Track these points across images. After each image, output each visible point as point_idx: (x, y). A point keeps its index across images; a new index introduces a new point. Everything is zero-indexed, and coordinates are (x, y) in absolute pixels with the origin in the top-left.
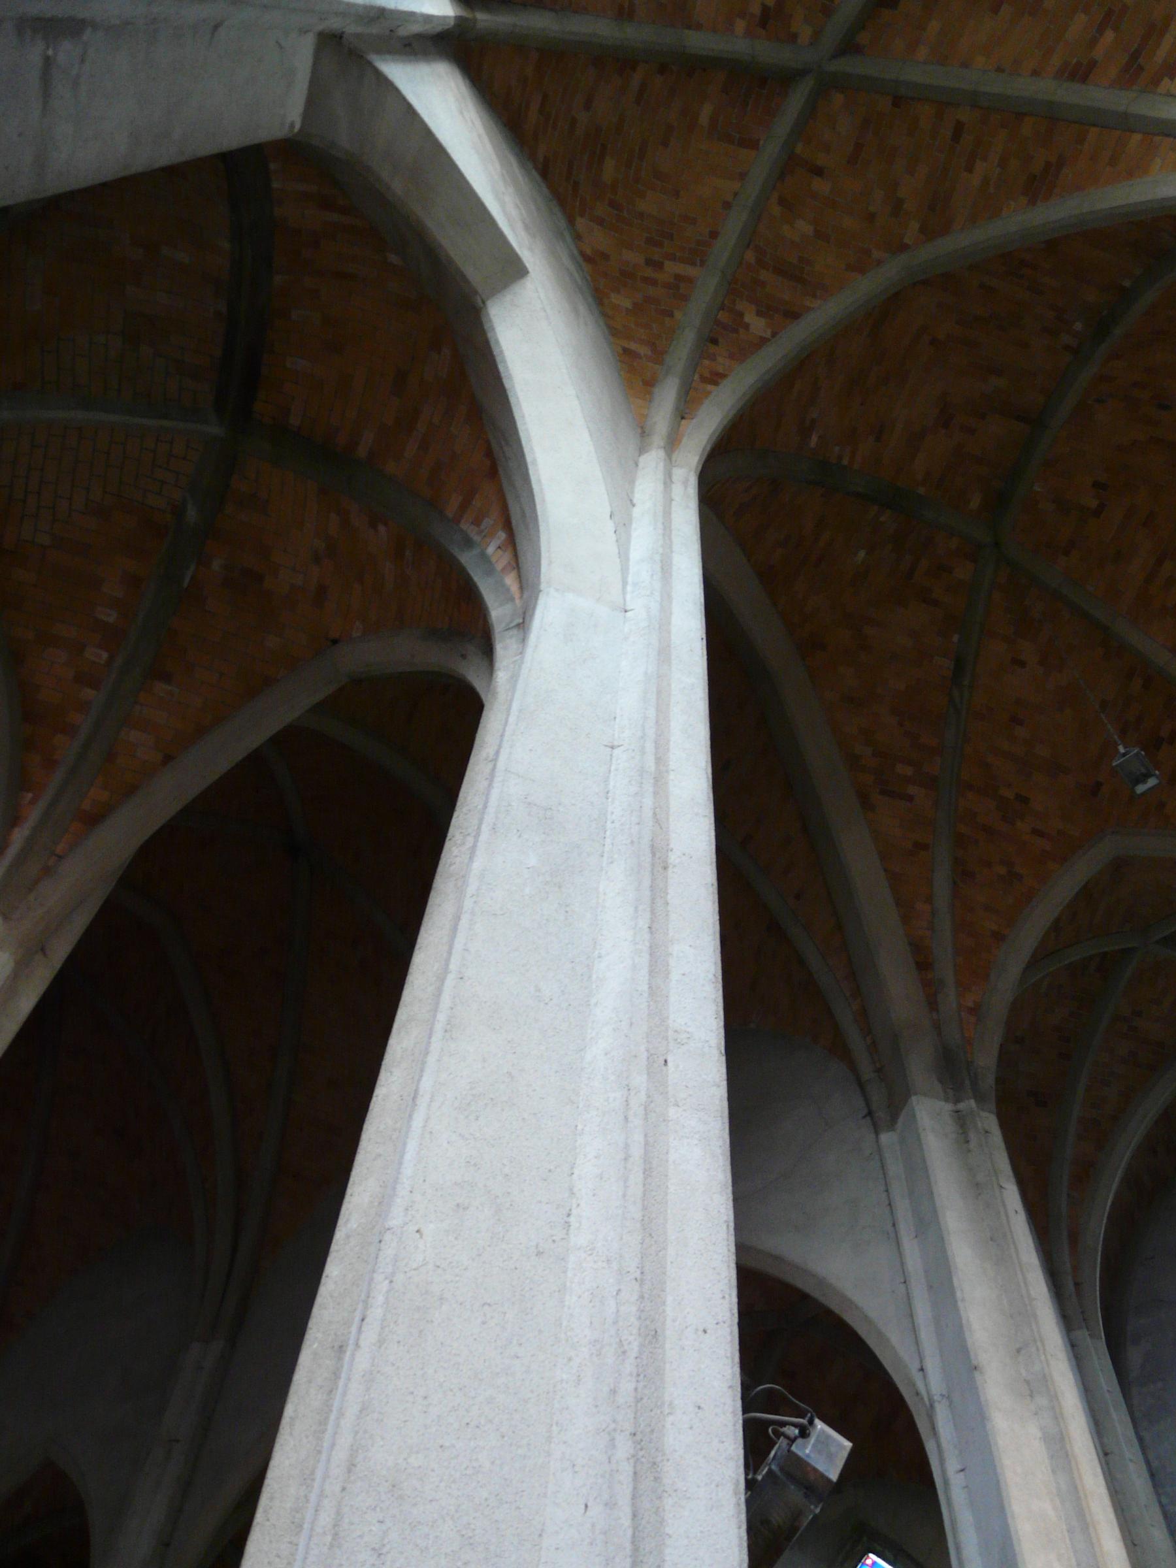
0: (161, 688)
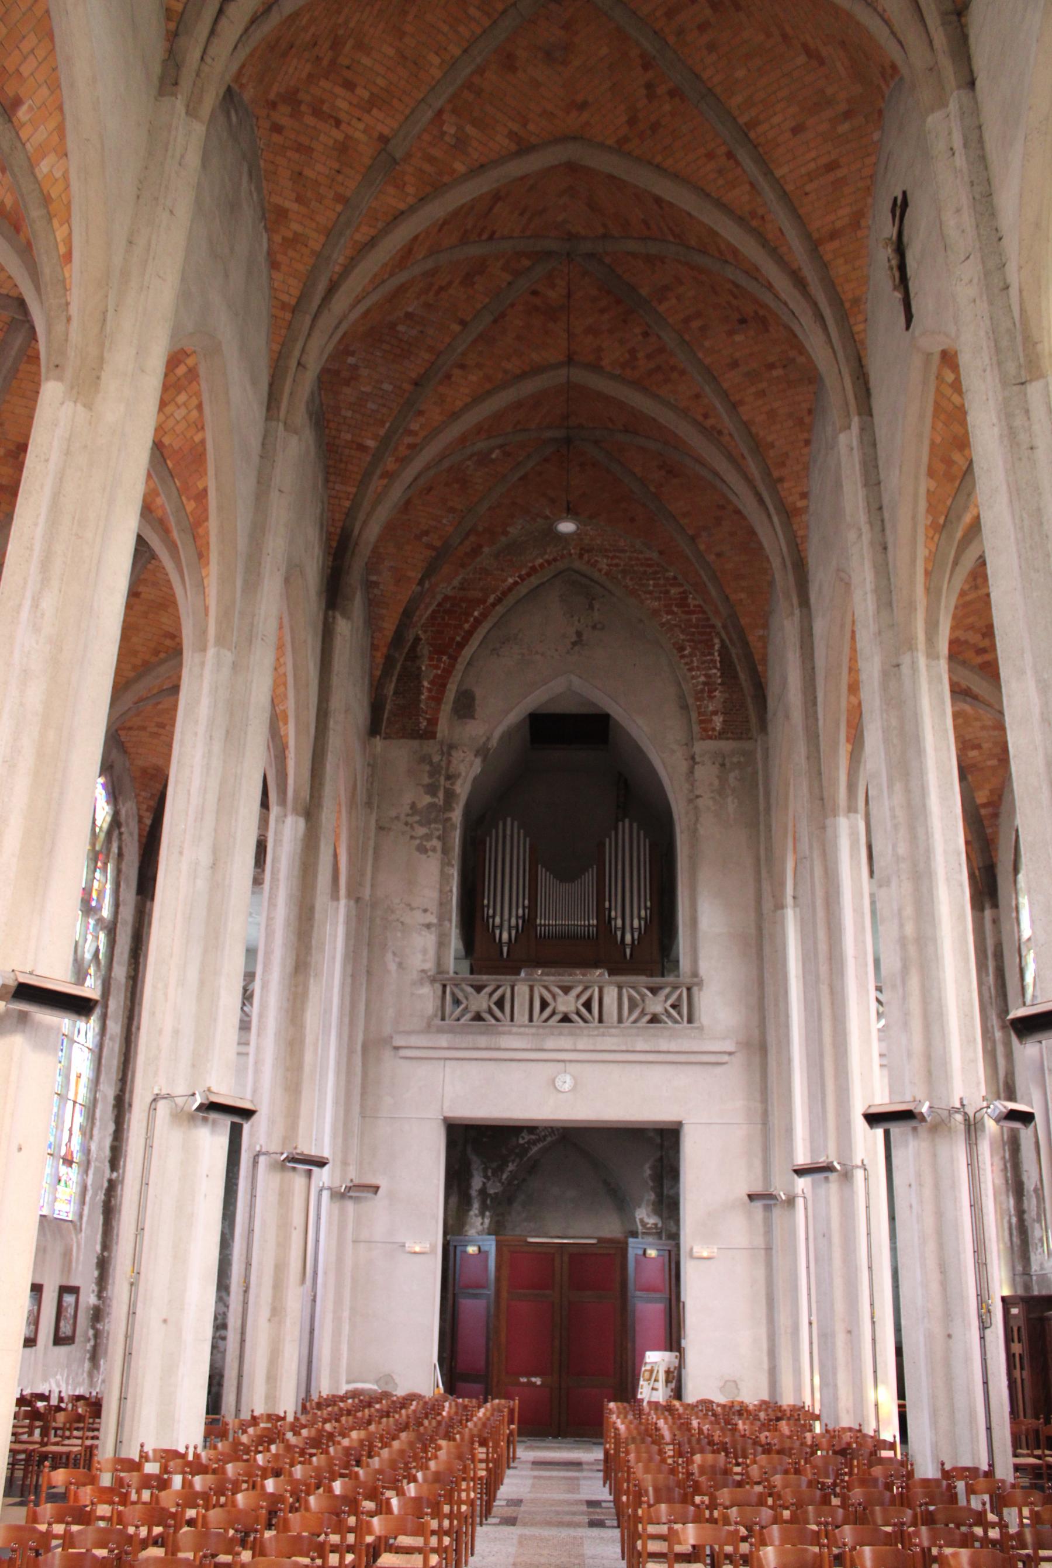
0: (22, 114)
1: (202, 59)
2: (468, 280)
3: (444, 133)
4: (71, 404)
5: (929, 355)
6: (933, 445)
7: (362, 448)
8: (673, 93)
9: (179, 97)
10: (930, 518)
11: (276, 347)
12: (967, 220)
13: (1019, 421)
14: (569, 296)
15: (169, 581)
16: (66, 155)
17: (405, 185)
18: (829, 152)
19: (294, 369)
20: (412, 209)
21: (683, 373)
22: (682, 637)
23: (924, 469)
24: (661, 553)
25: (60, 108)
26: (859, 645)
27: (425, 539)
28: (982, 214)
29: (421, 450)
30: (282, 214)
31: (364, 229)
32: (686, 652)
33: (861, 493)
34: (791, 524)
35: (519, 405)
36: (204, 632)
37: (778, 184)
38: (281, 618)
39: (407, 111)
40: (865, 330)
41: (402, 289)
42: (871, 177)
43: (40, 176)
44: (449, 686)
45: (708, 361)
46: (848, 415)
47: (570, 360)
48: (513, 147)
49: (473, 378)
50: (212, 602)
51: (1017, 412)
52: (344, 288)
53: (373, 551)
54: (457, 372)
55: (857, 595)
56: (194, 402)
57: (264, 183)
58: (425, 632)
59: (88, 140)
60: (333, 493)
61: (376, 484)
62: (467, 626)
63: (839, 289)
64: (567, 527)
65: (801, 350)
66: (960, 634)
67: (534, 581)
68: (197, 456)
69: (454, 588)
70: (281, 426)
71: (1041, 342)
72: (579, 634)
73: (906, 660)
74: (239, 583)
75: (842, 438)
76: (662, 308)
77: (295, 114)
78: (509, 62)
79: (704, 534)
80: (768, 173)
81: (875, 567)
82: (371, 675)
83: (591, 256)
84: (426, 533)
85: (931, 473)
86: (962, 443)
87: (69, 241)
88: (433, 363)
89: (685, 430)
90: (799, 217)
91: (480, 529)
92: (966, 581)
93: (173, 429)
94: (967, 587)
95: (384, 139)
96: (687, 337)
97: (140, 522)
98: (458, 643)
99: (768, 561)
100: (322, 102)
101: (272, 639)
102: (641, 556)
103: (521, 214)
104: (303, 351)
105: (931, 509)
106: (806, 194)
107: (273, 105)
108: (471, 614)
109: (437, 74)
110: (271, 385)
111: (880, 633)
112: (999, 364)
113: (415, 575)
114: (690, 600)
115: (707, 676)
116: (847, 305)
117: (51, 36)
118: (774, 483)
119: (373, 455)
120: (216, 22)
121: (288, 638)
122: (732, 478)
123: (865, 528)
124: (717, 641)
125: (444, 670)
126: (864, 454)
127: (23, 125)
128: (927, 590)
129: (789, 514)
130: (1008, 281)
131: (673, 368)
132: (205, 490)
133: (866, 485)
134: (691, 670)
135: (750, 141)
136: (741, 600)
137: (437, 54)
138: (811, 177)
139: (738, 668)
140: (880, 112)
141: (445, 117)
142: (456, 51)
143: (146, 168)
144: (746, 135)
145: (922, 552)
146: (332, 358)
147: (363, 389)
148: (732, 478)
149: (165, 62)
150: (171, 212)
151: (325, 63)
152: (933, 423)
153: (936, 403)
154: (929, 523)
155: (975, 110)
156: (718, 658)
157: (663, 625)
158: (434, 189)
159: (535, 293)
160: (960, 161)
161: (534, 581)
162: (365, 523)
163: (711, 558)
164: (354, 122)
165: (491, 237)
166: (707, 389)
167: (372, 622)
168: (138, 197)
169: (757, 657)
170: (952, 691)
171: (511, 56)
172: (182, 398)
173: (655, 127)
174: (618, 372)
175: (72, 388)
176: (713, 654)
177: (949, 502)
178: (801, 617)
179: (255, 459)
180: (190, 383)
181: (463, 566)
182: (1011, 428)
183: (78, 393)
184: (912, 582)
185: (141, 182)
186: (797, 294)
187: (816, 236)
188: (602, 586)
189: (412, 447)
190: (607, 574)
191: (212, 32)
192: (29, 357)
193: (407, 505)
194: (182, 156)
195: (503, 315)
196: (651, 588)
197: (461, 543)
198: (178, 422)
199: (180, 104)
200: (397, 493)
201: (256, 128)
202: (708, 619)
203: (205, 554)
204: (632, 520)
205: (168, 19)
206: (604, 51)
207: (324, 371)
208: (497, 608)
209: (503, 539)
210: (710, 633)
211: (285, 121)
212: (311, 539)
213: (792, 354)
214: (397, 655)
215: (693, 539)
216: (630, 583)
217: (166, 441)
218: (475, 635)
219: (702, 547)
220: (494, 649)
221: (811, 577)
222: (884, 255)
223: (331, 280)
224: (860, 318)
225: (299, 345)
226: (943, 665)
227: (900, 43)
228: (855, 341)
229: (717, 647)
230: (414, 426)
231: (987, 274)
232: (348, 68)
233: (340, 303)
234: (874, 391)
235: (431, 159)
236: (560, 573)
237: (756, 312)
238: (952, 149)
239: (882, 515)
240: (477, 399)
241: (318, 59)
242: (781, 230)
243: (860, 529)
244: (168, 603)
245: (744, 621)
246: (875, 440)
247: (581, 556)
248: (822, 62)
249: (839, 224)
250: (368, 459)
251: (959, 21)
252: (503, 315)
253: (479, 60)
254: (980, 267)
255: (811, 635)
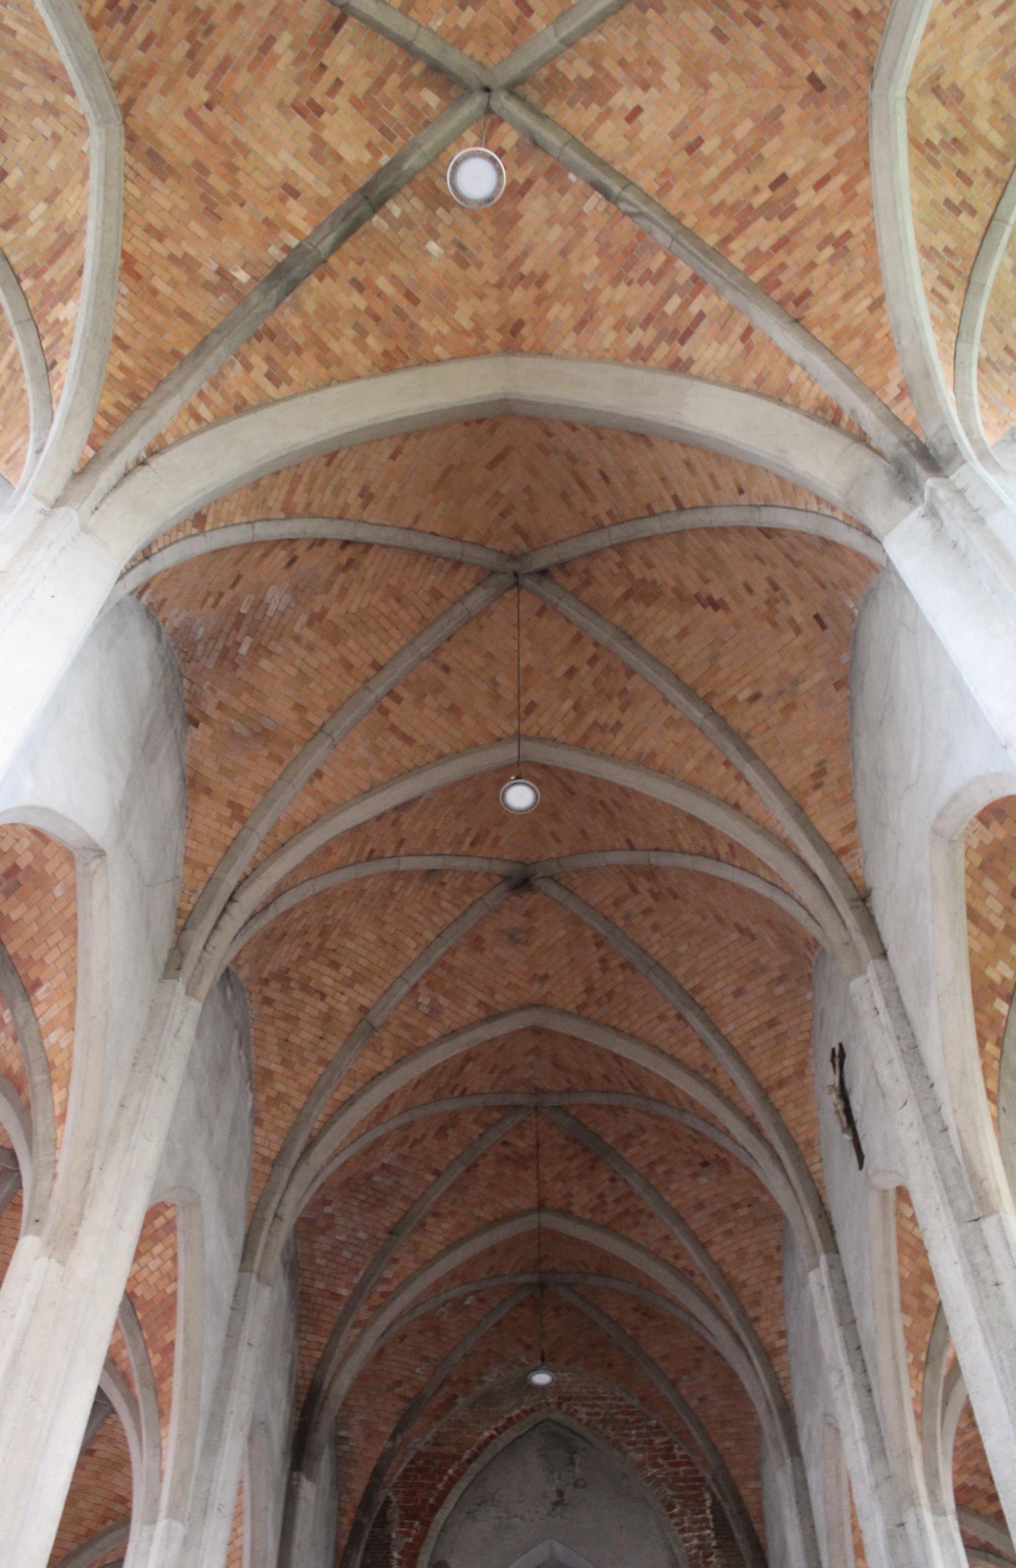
0: (40, 994)
1: (205, 948)
2: (442, 1132)
3: (419, 1004)
4: (46, 1259)
5: (885, 1192)
6: (902, 1280)
7: (335, 1296)
8: (624, 966)
9: (181, 979)
10: (911, 1356)
11: (254, 1199)
12: (899, 1069)
13: (980, 1258)
14: (538, 1145)
15: (125, 1437)
16: (73, 1029)
17: (383, 1048)
18: (768, 1011)
19: (271, 1219)
20: (389, 1070)
21: (651, 1215)
22: (670, 1493)
23: (896, 1305)
24: (642, 1399)
25: (74, 990)
26: (858, 1502)
27: (398, 1390)
28: (912, 1064)
29: (394, 1299)
30: (268, 1075)
31: (344, 1089)
32: (675, 1511)
33: (837, 1333)
34: (772, 1366)
35: (492, 1251)
36: (157, 1500)
37: (725, 1040)
38: (241, 1482)
39: (386, 986)
40: (821, 1170)
41: (378, 1142)
42: (809, 1031)
43: (47, 1046)
44: (421, 1558)
45: (674, 1204)
46: (815, 1253)
47: (541, 1206)
48: (482, 1015)
49: (446, 1226)
50: (168, 1465)
51: (976, 1248)
52: (324, 1142)
53: (344, 1404)
54: (431, 1220)
55: (847, 1444)
56: (170, 1253)
57: (253, 1048)
58: (396, 1493)
59: (94, 1017)
60: (305, 1343)
61: (349, 1333)
62: (440, 1486)
63: (793, 1133)
64: (541, 1378)
65: (764, 1190)
66: (965, 1478)
67: (511, 1434)
68: (168, 1308)
69: (427, 1443)
70: (254, 1276)
71: (987, 1179)
72: (560, 1493)
73: (910, 1518)
74: (199, 1444)
75: (812, 1276)
76: (626, 1155)
77: (286, 989)
78: (477, 944)
79: (685, 1378)
80: (716, 1031)
81: (862, 1412)
82: (337, 1544)
83: (558, 1108)
84: (399, 1383)
85: (905, 1308)
86: (928, 1276)
87: (65, 1103)
88: (407, 1212)
89: (657, 1273)
90: (748, 1068)
91: (455, 1378)
92: (961, 1419)
93: (145, 1279)
94: (963, 1425)
95: (364, 1010)
96: (653, 1182)
97: (102, 1374)
98: (432, 1505)
99: (752, 1405)
100: (310, 978)
101: (228, 1510)
102: (622, 1404)
103: (491, 1072)
104: (280, 1202)
105: (910, 1346)
106: (752, 1048)
107: (266, 982)
108: (444, 1472)
109: (414, 955)
110: (247, 1236)
111: (877, 1486)
112: (951, 1202)
113: (387, 1429)
114: (675, 1451)
115: (701, 1538)
116: (802, 1147)
117: (75, 933)
118: (751, 1323)
119: (347, 1304)
120: (220, 918)
121: (247, 1505)
122: (707, 1317)
123: (847, 1370)
124: (707, 1496)
125: (416, 1538)
126: (836, 1292)
127: (39, 1003)
128: (920, 1434)
129: (769, 1355)
130: (946, 1123)
131: (642, 1211)
132: (172, 1344)
133: (841, 1324)
134: (683, 1531)
135: (696, 1004)
136: (729, 1449)
137: (413, 938)
138: (755, 1032)
139: (734, 1527)
140: (810, 976)
141: (420, 990)
142: (430, 936)
143: (144, 1040)
144: (693, 999)
145: (908, 1394)
146: (309, 1208)
147: (338, 1237)
148: (707, 1317)
149: (172, 951)
150: (163, 1078)
151: (313, 948)
152: (899, 1257)
153: (899, 1239)
154: (910, 1360)
155: (892, 977)
156: (710, 1517)
157: (649, 1479)
158: (410, 1052)
159: (505, 1143)
160: (884, 1018)
161: (511, 1434)
162: (336, 1375)
163: (694, 1403)
164: (338, 996)
165: (463, 1094)
166: (676, 1230)
167: (339, 1482)
168: (134, 1065)
169: (753, 1513)
170: (967, 1547)
171: (479, 939)
172: (158, 1249)
173: (610, 995)
174: (588, 1216)
175: (49, 1243)
176: (703, 1512)
177: (927, 1338)
178: (793, 1465)
179: (226, 1311)
180: (168, 1234)
181: (437, 1418)
182: (972, 1265)
183: (54, 1249)
184: (903, 1430)
185: (138, 1052)
186: (752, 1137)
187: (765, 1085)
188: (582, 1438)
189: (384, 1295)
190: (587, 1424)
191: (215, 927)
192: (14, 1204)
193: (380, 1354)
194: (178, 1030)
195: (475, 1165)
196: (634, 1439)
197: (434, 1394)
198: (152, 1273)
199: (180, 986)
200: (369, 1343)
201: (248, 1002)
202: (696, 1471)
203: (166, 1412)
204: (610, 1365)
205: (179, 917)
206: (562, 933)
207: (301, 1220)
208: (472, 1465)
209: (478, 1388)
210: (700, 1486)
211: (277, 996)
212: (280, 1389)
213: (756, 1193)
214: (365, 1520)
215: (674, 1383)
216: (612, 1434)
217: (138, 1291)
218: (449, 1496)
219: (684, 1392)
220: (468, 1513)
221: (799, 1420)
222: (831, 1101)
223: (310, 1136)
224: (816, 1159)
225: (277, 1198)
226: (952, 1523)
227: (817, 922)
228: (813, 1181)
229: (708, 1503)
230: (388, 1274)
231: (925, 1118)
232: (334, 951)
233: (319, 1157)
234: (837, 1228)
235: (407, 1026)
236: (537, 1425)
237: (717, 1155)
238: (876, 1009)
239: (861, 1354)
240: (451, 1247)
241: (308, 945)
242: (732, 1081)
243: (841, 1371)
244: (122, 1463)
245: (735, 1472)
246: (844, 1277)
247: (559, 1405)
248: (753, 938)
249: (784, 1074)
250: (341, 1308)
251: (865, 905)
252: (475, 1165)
253: (450, 943)
254: (918, 1112)
255: (806, 1488)
